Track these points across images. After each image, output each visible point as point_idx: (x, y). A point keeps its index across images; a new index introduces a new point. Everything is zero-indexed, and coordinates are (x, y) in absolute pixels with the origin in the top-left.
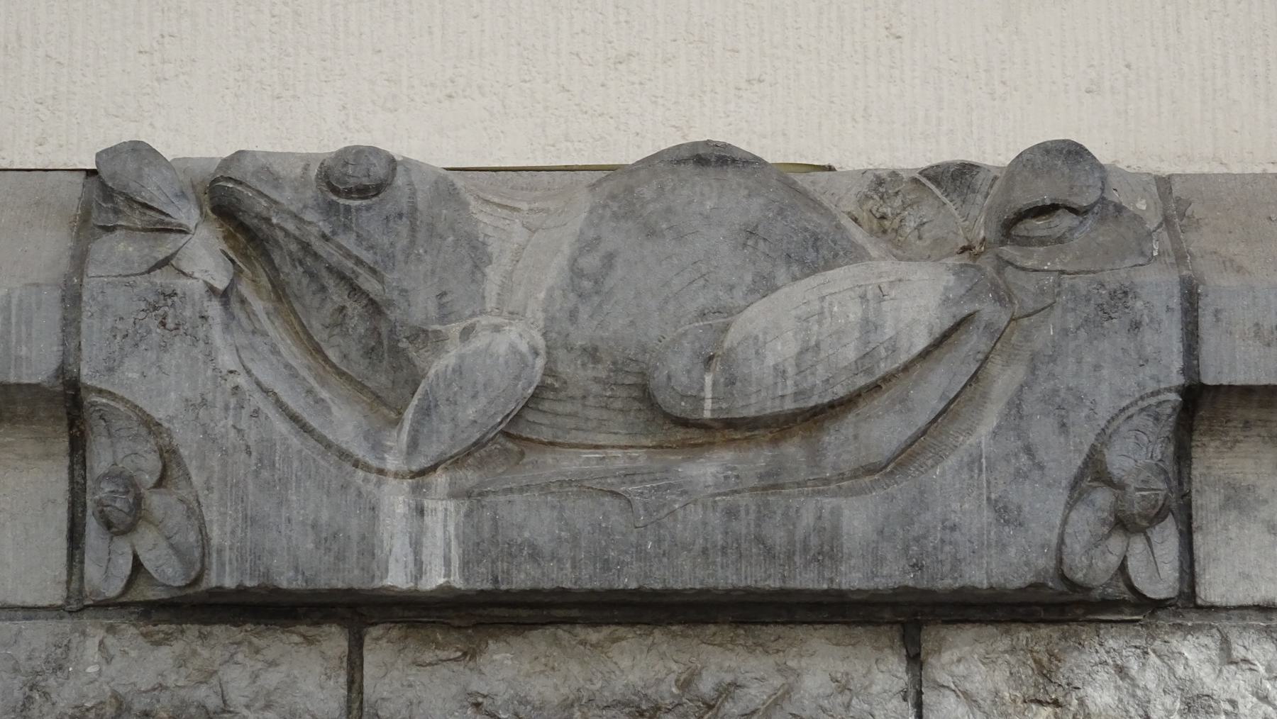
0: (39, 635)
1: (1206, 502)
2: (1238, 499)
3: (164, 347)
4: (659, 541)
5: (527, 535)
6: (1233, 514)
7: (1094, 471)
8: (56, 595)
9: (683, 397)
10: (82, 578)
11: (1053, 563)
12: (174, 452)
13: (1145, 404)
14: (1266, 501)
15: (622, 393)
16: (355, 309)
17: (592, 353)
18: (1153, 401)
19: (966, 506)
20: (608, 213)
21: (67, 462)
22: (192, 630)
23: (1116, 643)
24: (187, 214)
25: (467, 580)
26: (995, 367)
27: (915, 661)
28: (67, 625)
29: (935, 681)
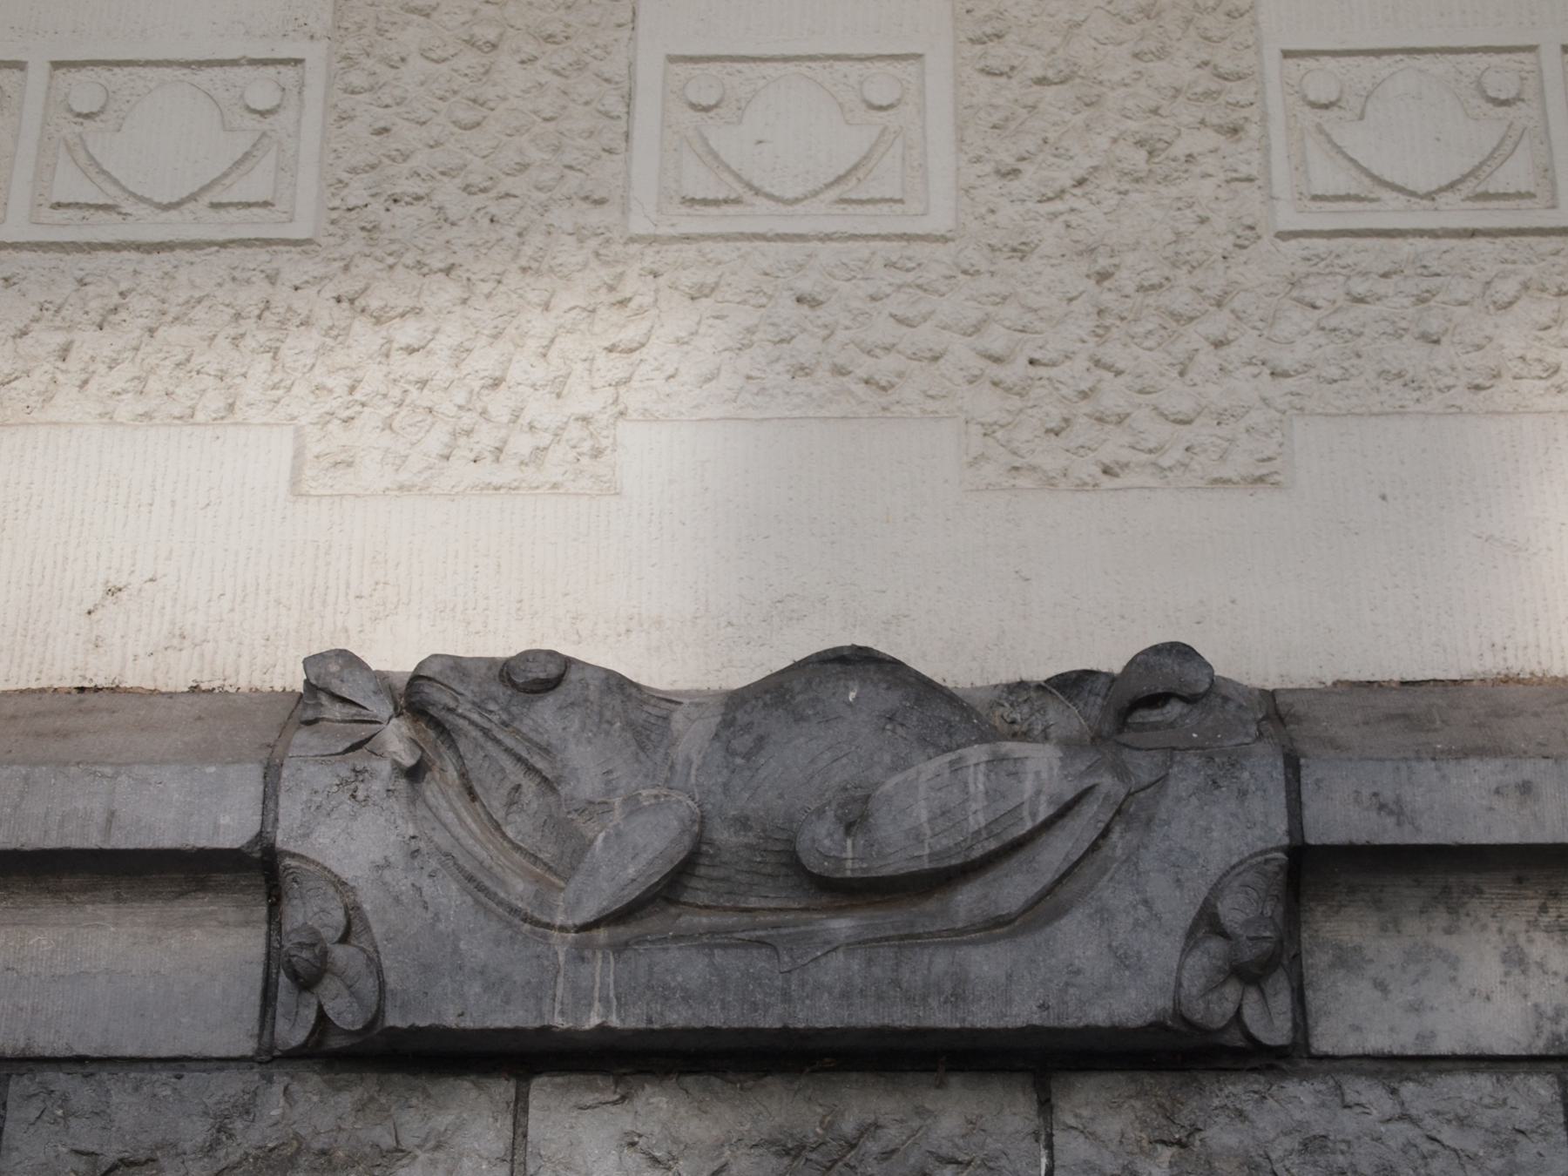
0: (232, 1085)
1: (1317, 962)
2: (1347, 960)
3: (354, 817)
4: (803, 984)
5: (680, 979)
6: (1342, 972)
7: (1208, 922)
8: (247, 1047)
9: (827, 857)
10: (272, 1033)
11: (1170, 1004)
12: (357, 908)
13: (1253, 861)
14: (1371, 961)
15: (771, 859)
16: (530, 786)
17: (743, 823)
18: (1260, 859)
19: (1089, 953)
20: (761, 703)
21: (264, 928)
22: (372, 1079)
23: (1237, 1090)
24: (380, 708)
25: (623, 1021)
26: (1117, 830)
27: (1046, 1106)
28: (254, 1076)
29: (1064, 1123)
